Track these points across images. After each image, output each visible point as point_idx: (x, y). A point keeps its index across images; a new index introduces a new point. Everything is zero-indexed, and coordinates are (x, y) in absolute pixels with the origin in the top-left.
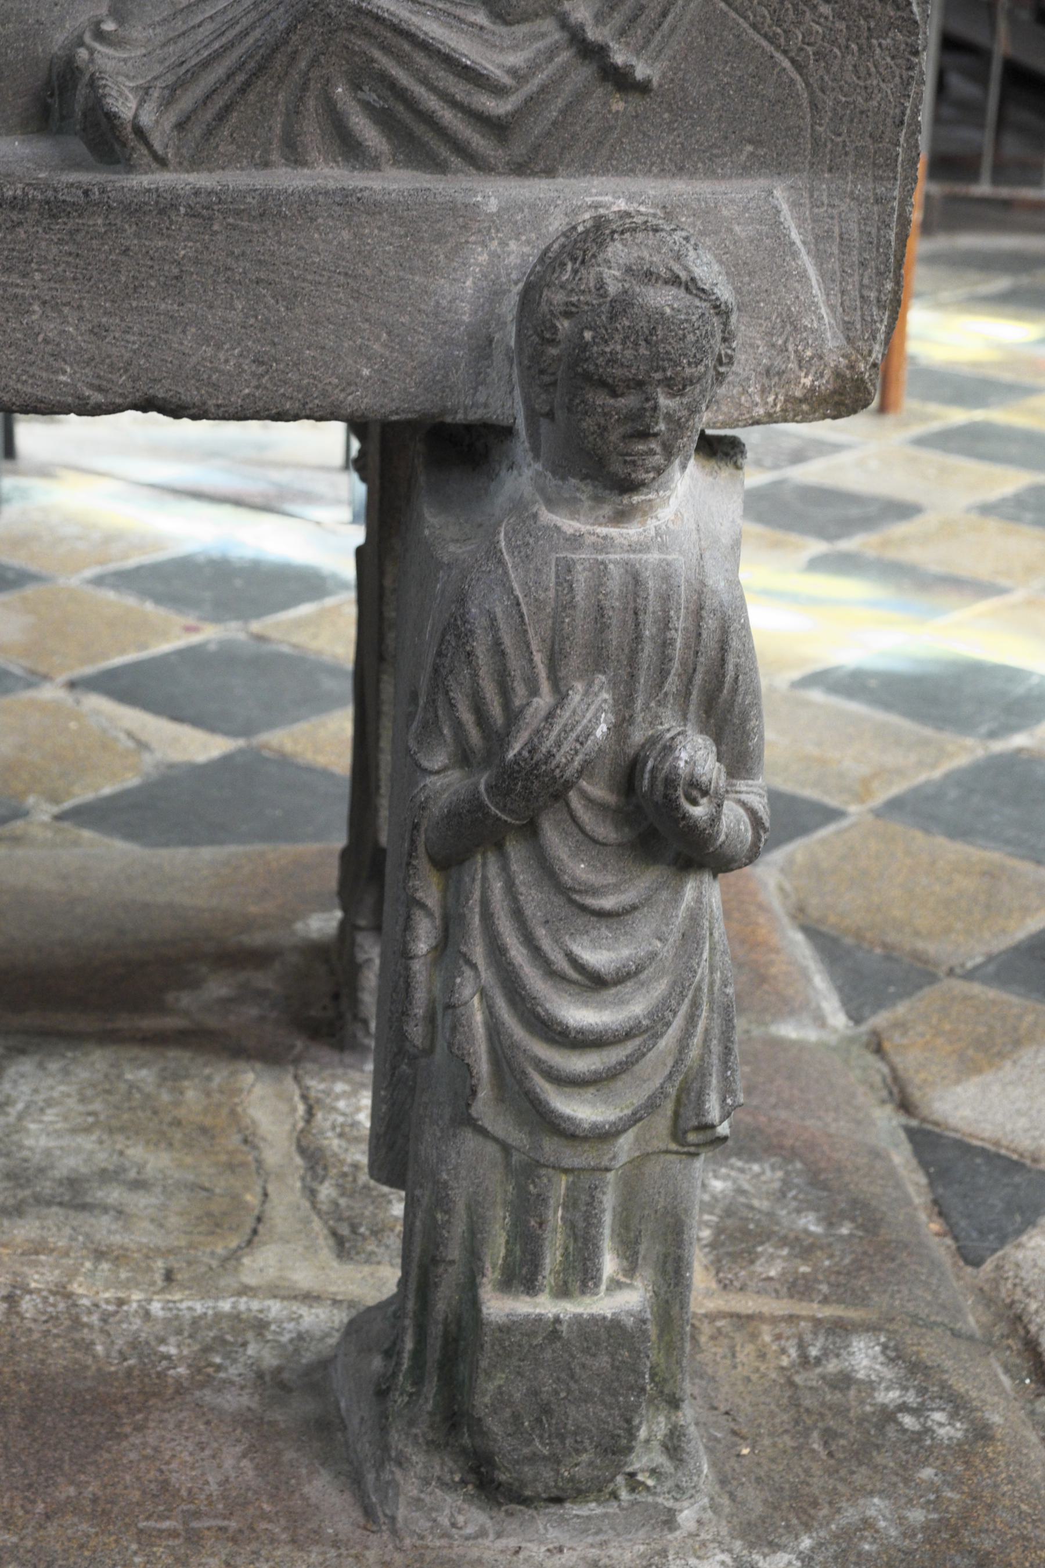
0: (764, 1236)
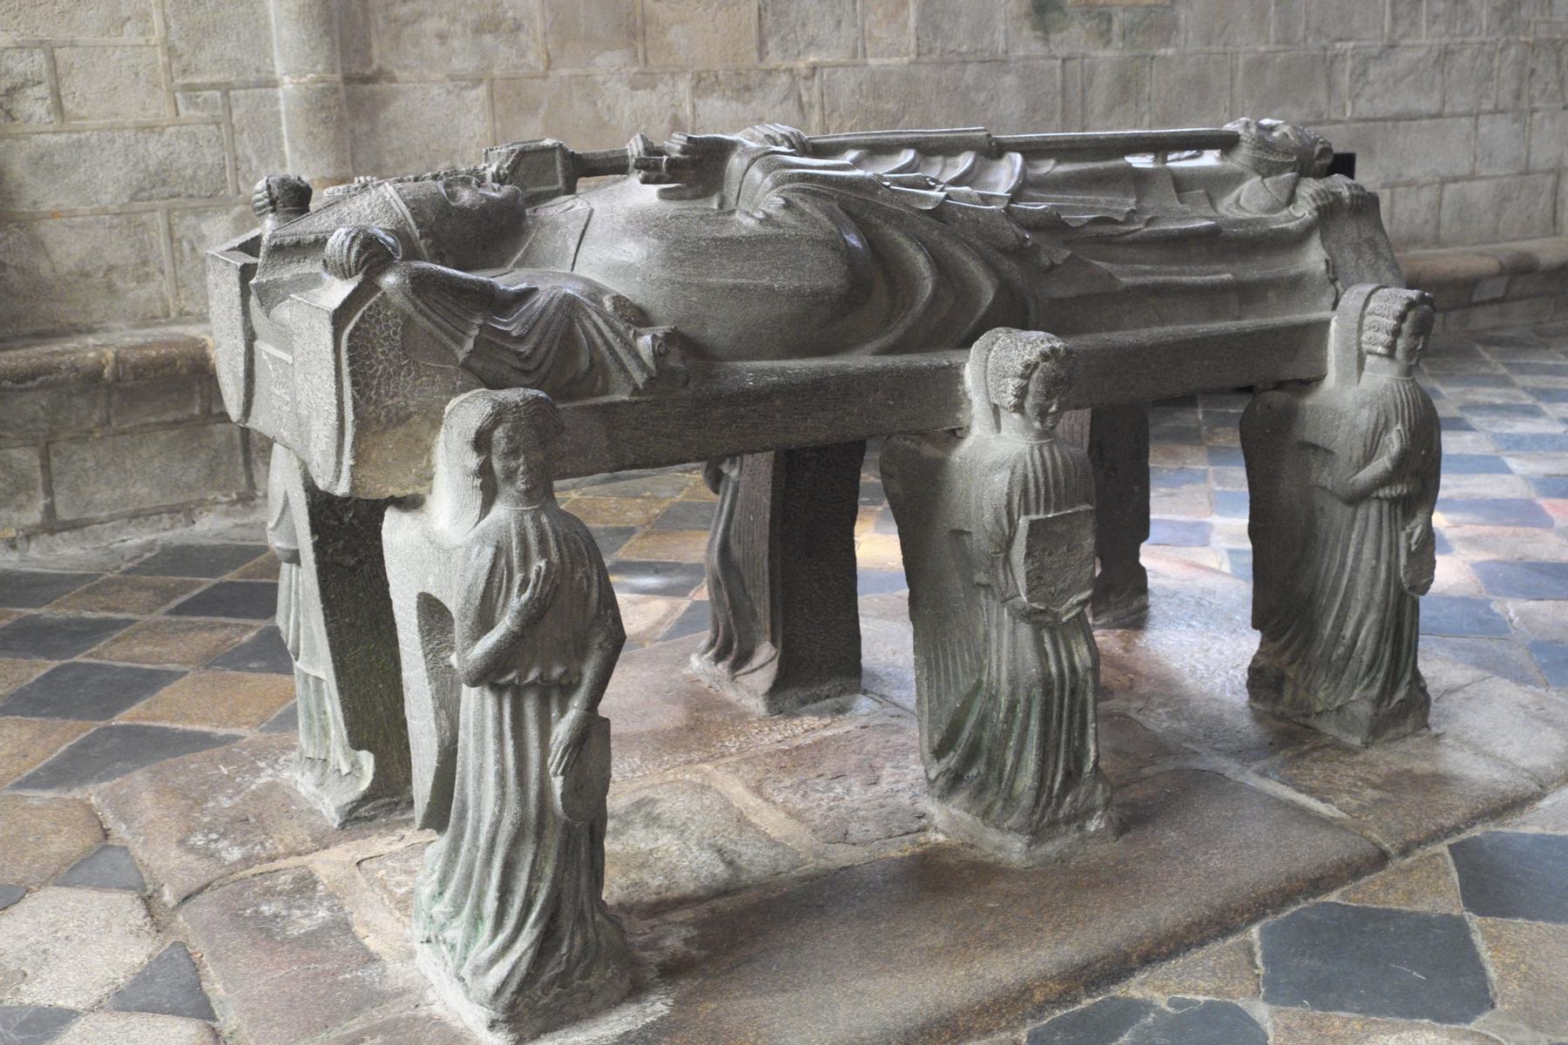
0: (290, 894)
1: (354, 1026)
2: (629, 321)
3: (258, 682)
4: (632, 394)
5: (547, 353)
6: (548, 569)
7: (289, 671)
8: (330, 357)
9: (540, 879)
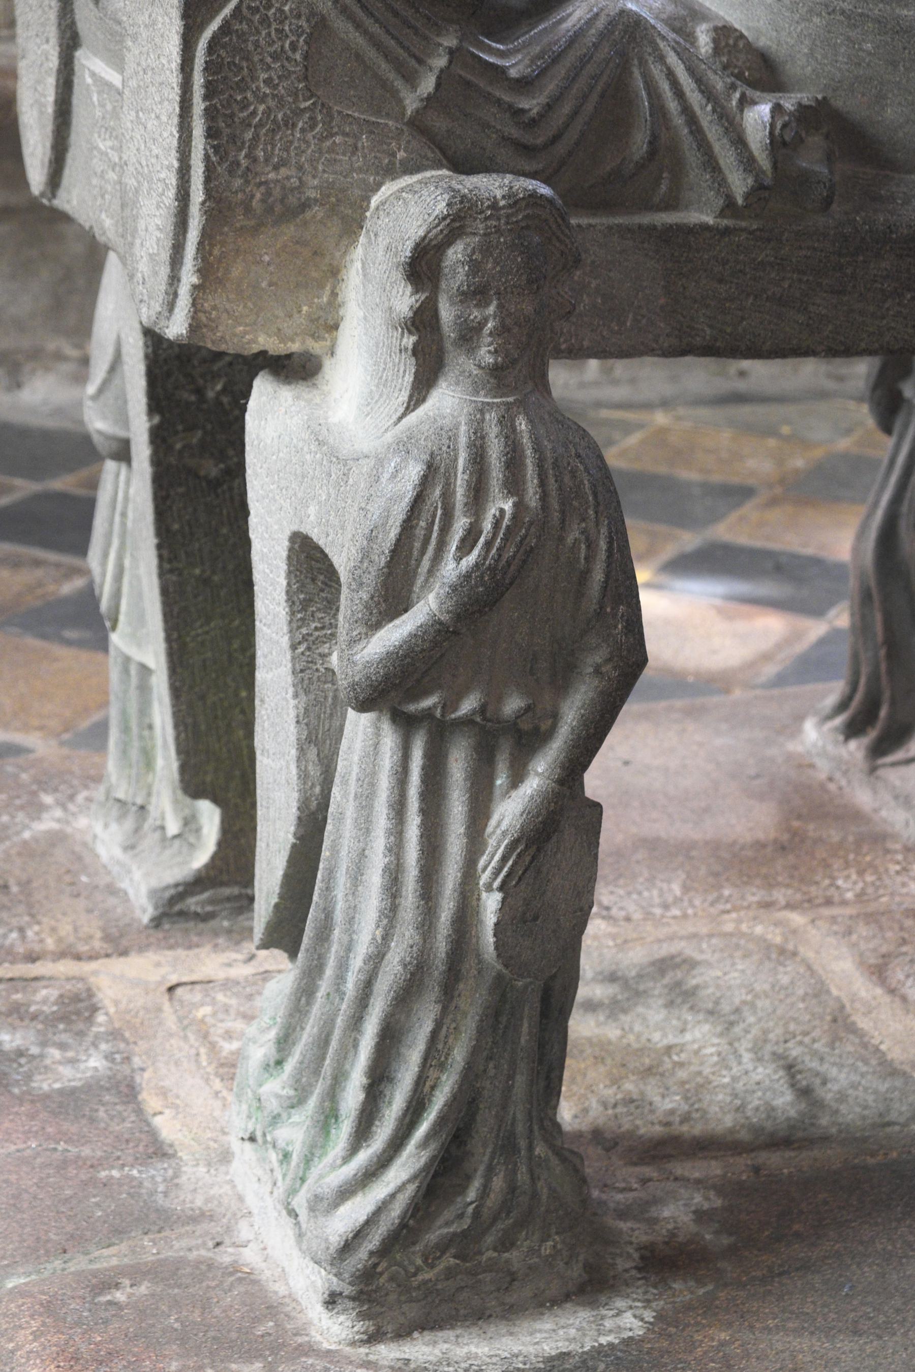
0: (52, 1021)
1: (110, 1258)
2: (739, 76)
3: (68, 659)
4: (722, 214)
5: (575, 113)
6: (515, 517)
7: (102, 644)
8: (174, 79)
9: (442, 1067)
